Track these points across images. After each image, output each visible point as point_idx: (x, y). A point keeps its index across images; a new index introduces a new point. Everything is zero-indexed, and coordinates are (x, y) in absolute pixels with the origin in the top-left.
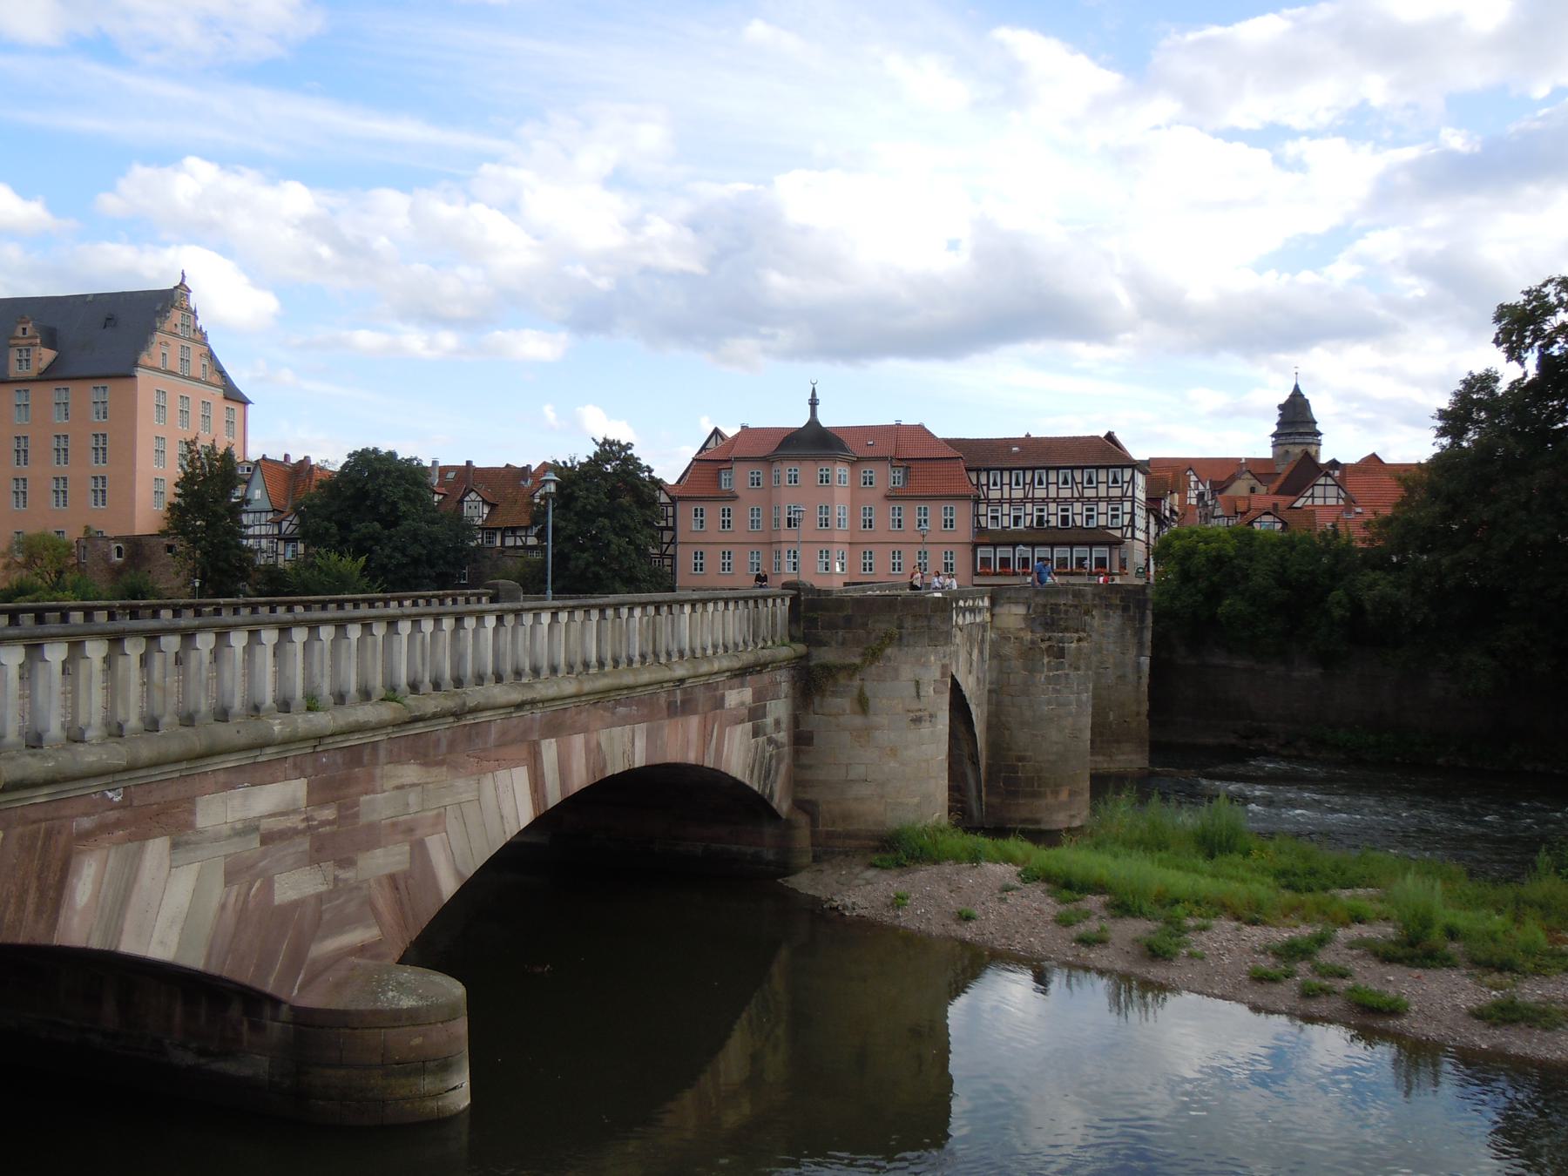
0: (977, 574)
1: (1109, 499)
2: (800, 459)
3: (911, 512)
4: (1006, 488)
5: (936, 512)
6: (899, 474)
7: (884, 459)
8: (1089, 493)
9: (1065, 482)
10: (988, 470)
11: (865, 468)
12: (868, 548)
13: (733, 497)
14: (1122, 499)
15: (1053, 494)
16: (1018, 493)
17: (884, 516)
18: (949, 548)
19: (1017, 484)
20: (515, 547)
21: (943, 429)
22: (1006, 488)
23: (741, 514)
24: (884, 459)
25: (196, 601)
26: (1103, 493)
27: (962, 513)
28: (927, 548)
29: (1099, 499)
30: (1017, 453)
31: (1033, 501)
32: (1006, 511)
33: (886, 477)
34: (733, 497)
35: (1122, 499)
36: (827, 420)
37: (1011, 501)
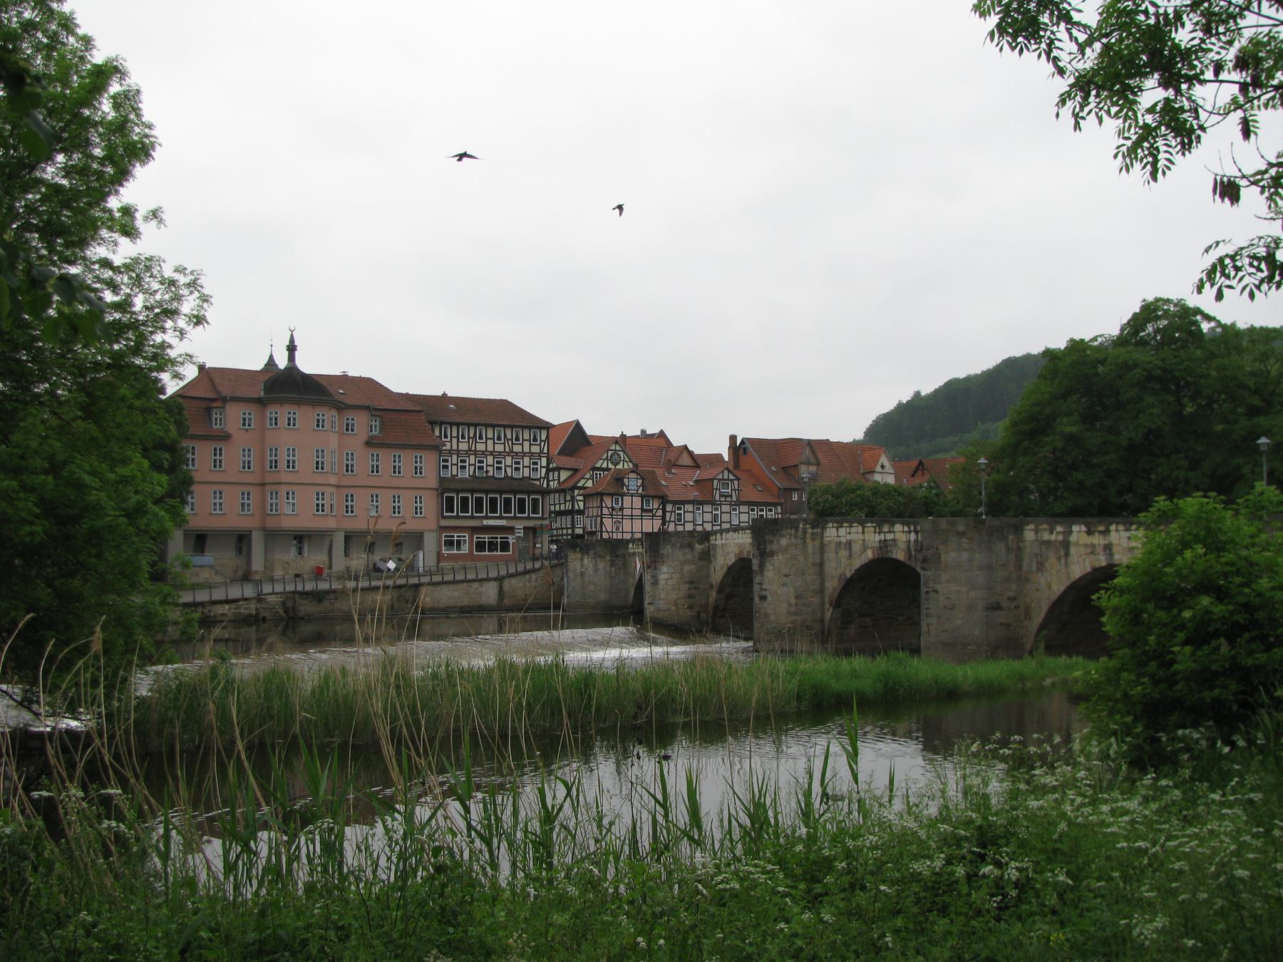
0: (444, 517)
1: (531, 454)
2: (299, 403)
3: (386, 459)
4: (455, 440)
5: (407, 460)
6: (376, 423)
7: (367, 408)
8: (517, 448)
9: (499, 438)
10: (441, 424)
11: (350, 415)
12: (349, 491)
13: (226, 437)
14: (540, 455)
15: (490, 448)
16: (463, 446)
17: (363, 460)
18: (419, 493)
19: (463, 437)
20: (677, 533)
21: (397, 384)
22: (455, 440)
23: (233, 455)
24: (367, 408)
25: (388, 750)
26: (526, 449)
27: (429, 462)
28: (401, 492)
29: (524, 454)
30: (452, 410)
31: (476, 453)
32: (454, 461)
33: (363, 425)
34: (226, 437)
35: (540, 455)
36: (307, 365)
37: (458, 452)
